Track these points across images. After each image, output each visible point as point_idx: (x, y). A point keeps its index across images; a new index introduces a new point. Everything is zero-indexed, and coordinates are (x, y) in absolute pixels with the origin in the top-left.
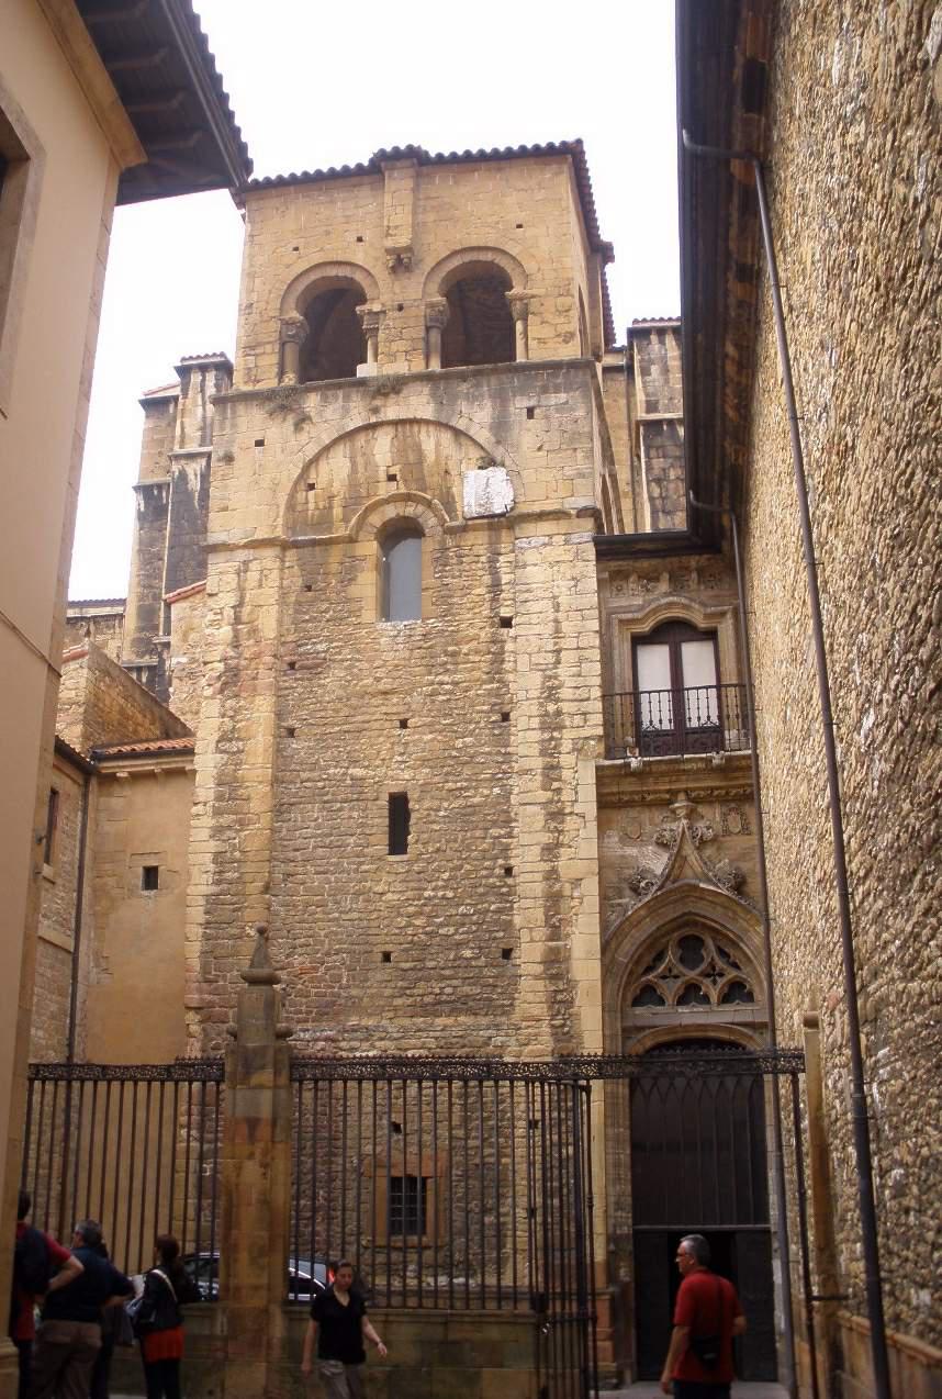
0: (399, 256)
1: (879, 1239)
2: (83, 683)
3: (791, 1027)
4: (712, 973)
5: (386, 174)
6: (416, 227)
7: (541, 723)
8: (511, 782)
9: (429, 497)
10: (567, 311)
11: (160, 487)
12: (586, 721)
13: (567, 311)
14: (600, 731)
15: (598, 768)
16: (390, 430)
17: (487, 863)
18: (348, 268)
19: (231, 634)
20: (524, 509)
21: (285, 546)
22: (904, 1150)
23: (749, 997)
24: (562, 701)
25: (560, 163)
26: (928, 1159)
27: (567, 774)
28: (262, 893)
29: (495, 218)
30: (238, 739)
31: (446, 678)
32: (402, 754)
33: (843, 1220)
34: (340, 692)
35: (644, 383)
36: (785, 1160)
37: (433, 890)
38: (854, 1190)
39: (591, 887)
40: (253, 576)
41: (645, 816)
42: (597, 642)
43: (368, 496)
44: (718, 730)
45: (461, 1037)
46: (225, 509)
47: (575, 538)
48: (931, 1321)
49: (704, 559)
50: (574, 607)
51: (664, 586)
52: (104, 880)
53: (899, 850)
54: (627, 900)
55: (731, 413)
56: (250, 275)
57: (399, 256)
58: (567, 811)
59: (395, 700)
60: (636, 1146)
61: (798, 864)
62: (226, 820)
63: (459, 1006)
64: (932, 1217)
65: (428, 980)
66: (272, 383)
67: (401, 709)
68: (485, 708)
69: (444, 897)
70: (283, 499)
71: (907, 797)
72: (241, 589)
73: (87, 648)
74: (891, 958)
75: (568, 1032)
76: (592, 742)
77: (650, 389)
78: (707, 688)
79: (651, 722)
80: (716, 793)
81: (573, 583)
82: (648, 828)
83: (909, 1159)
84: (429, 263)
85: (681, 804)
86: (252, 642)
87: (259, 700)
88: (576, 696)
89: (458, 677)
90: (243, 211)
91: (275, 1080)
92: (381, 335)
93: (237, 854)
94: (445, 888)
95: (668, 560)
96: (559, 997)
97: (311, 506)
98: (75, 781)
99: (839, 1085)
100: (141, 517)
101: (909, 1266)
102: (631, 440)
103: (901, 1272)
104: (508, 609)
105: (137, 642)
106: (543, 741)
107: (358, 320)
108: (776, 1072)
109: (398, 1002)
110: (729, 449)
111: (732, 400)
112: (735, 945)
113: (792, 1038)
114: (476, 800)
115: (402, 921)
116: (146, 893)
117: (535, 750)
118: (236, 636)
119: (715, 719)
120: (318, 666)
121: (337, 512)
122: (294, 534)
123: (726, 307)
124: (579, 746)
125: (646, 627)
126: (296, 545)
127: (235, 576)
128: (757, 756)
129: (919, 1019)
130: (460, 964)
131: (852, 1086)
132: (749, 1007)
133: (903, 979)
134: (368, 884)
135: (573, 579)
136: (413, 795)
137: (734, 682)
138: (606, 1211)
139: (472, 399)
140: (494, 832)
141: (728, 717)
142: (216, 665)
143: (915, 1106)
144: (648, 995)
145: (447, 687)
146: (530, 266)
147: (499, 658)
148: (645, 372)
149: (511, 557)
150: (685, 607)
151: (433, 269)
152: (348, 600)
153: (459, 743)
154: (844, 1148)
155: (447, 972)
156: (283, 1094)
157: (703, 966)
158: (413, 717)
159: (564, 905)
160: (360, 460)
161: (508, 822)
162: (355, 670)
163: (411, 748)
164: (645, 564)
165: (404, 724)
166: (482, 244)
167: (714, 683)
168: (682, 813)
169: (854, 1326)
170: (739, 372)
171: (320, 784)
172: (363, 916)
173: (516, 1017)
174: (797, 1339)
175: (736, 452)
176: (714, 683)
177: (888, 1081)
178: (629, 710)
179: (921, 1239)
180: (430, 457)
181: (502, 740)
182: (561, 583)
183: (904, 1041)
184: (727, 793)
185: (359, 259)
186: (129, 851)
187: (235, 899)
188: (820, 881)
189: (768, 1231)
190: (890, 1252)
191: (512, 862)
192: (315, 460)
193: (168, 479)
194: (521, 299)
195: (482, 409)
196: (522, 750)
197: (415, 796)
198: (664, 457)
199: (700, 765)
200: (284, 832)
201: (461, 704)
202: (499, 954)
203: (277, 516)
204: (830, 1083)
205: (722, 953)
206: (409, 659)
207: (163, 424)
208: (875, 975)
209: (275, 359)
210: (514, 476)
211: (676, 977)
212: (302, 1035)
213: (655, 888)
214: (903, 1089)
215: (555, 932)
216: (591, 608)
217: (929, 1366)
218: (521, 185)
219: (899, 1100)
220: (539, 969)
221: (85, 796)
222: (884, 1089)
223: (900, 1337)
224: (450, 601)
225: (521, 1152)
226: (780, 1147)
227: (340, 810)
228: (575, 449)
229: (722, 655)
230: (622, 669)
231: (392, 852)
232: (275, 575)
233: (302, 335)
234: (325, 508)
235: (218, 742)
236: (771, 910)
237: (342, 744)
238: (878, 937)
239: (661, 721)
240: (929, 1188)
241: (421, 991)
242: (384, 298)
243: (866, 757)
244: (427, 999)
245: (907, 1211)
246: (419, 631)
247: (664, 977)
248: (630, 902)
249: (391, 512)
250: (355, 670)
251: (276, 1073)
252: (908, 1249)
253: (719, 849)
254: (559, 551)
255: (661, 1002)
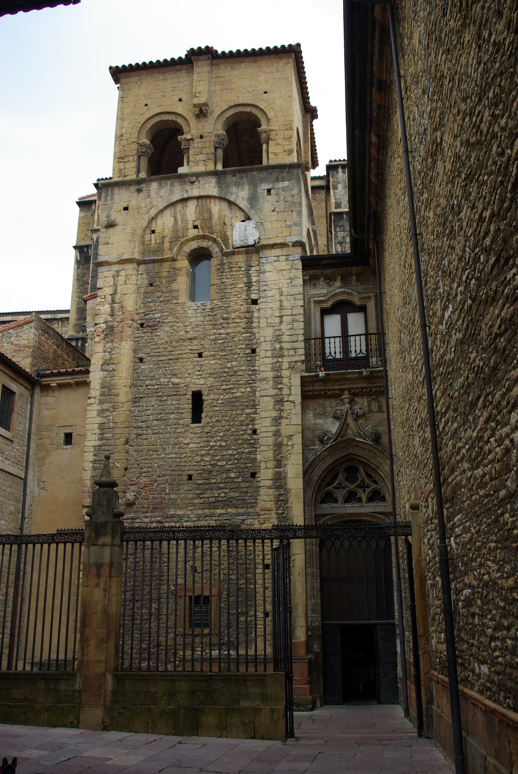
0: (201, 109)
1: (455, 632)
2: (32, 336)
3: (404, 513)
4: (363, 486)
5: (195, 63)
6: (210, 92)
7: (272, 354)
8: (256, 385)
9: (215, 237)
10: (290, 138)
11: (88, 247)
12: (296, 352)
13: (290, 138)
14: (303, 358)
15: (302, 377)
16: (195, 202)
17: (243, 428)
18: (174, 116)
19: (110, 309)
20: (264, 242)
21: (139, 263)
22: (471, 577)
23: (383, 499)
24: (283, 342)
25: (288, 58)
26: (488, 583)
27: (285, 380)
28: (124, 444)
29: (253, 88)
30: (113, 364)
31: (222, 331)
32: (199, 371)
33: (434, 620)
34: (167, 339)
35: (334, 193)
36: (403, 585)
37: (215, 442)
38: (440, 602)
39: (298, 439)
40: (121, 279)
41: (327, 402)
42: (302, 312)
43: (183, 237)
44: (366, 358)
45: (229, 519)
46: (108, 243)
47: (291, 258)
48: (488, 684)
49: (360, 269)
50: (290, 294)
51: (338, 284)
52: (44, 440)
53: (468, 386)
54: (317, 447)
55: (373, 179)
56: (121, 118)
57: (201, 109)
58: (285, 400)
59: (195, 343)
60: (323, 580)
61: (408, 419)
62: (105, 406)
63: (227, 503)
64: (491, 620)
65: (211, 489)
66: (134, 177)
67: (199, 347)
68: (243, 346)
69: (220, 446)
70: (138, 238)
71: (474, 349)
72: (115, 286)
73: (33, 318)
74: (462, 458)
75: (286, 517)
76: (299, 364)
77: (337, 197)
78: (360, 335)
79: (330, 353)
80: (365, 390)
81: (290, 281)
82: (329, 409)
83: (475, 583)
84: (217, 112)
85: (346, 396)
86: (121, 313)
87: (124, 343)
88: (291, 340)
89: (229, 331)
90: (118, 85)
91: (112, 541)
92: (191, 152)
93: (111, 424)
94: (220, 440)
95: (341, 269)
96: (281, 498)
97: (153, 242)
98: (26, 388)
99: (431, 541)
100: (78, 263)
101: (474, 650)
102: (327, 223)
103: (469, 652)
104: (255, 295)
105: (76, 325)
106: (273, 363)
107: (179, 144)
108: (396, 535)
109: (196, 501)
110: (373, 202)
111: (374, 171)
112: (375, 471)
113: (405, 518)
114: (238, 394)
115: (198, 459)
116: (65, 447)
117: (269, 367)
118: (112, 310)
119: (364, 351)
120: (155, 326)
121: (167, 245)
122: (144, 256)
123: (371, 110)
124: (292, 365)
125: (329, 305)
126: (144, 262)
127: (112, 279)
128: (386, 371)
129: (481, 493)
130: (229, 481)
131: (439, 541)
132: (383, 504)
133: (469, 469)
134: (181, 439)
135: (290, 278)
136: (205, 392)
137: (375, 332)
138: (306, 614)
139: (238, 185)
140: (247, 411)
141: (371, 350)
142: (102, 325)
143: (479, 549)
144: (329, 498)
145: (223, 336)
146: (270, 115)
147: (250, 321)
148: (335, 188)
149: (257, 268)
150: (349, 294)
151: (219, 116)
152: (172, 291)
153: (229, 365)
154: (434, 578)
155: (222, 485)
156: (117, 549)
157: (358, 482)
158: (205, 351)
159: (284, 449)
160: (179, 217)
161: (254, 406)
162: (175, 328)
163: (204, 368)
164: (328, 271)
165: (200, 355)
166: (245, 102)
167: (364, 332)
168: (347, 401)
169: (440, 681)
170: (378, 153)
171: (156, 387)
172: (177, 456)
173: (258, 509)
174: (408, 682)
175: (377, 203)
176: (364, 332)
177: (461, 535)
178: (319, 346)
179: (483, 633)
180: (216, 216)
181: (251, 363)
182: (283, 281)
183: (471, 508)
184: (371, 390)
185: (179, 111)
186: (57, 425)
187: (110, 448)
188: (419, 425)
189: (394, 624)
190: (462, 640)
191: (257, 427)
192: (154, 218)
193: (91, 243)
194: (266, 132)
195: (243, 190)
196: (262, 368)
197: (206, 393)
198: (344, 231)
199: (357, 375)
200: (136, 413)
201: (230, 344)
202: (249, 475)
203: (135, 247)
204: (425, 540)
205: (369, 476)
206: (203, 322)
207: (89, 214)
208: (452, 471)
209: (134, 164)
210: (260, 225)
211: (344, 488)
212: (144, 519)
213: (332, 440)
214: (471, 539)
215: (279, 463)
216: (299, 294)
217: (486, 712)
218: (266, 70)
219: (468, 546)
220: (270, 483)
221: (32, 396)
222: (458, 540)
223: (467, 691)
224: (225, 291)
225: (260, 582)
226: (399, 578)
227: (166, 400)
228: (292, 211)
229: (368, 319)
230: (316, 327)
231: (194, 422)
232: (134, 278)
233: (150, 152)
234: (160, 243)
235: (102, 365)
236: (394, 451)
237: (167, 366)
238: (454, 446)
239: (335, 353)
240: (489, 601)
241: (208, 496)
242: (193, 132)
243: (446, 338)
244: (211, 500)
245: (473, 615)
246: (209, 307)
247: (337, 488)
248: (318, 447)
249: (194, 245)
250: (175, 328)
251: (113, 538)
252: (474, 639)
253: (366, 420)
254: (283, 265)
255: (336, 501)
